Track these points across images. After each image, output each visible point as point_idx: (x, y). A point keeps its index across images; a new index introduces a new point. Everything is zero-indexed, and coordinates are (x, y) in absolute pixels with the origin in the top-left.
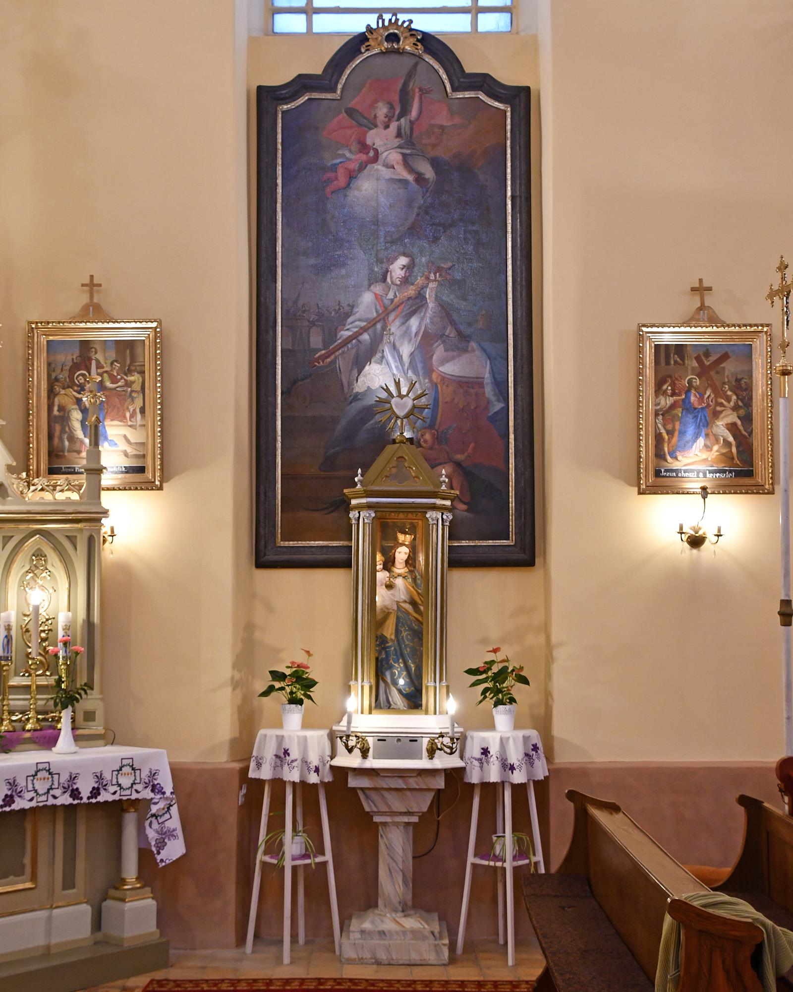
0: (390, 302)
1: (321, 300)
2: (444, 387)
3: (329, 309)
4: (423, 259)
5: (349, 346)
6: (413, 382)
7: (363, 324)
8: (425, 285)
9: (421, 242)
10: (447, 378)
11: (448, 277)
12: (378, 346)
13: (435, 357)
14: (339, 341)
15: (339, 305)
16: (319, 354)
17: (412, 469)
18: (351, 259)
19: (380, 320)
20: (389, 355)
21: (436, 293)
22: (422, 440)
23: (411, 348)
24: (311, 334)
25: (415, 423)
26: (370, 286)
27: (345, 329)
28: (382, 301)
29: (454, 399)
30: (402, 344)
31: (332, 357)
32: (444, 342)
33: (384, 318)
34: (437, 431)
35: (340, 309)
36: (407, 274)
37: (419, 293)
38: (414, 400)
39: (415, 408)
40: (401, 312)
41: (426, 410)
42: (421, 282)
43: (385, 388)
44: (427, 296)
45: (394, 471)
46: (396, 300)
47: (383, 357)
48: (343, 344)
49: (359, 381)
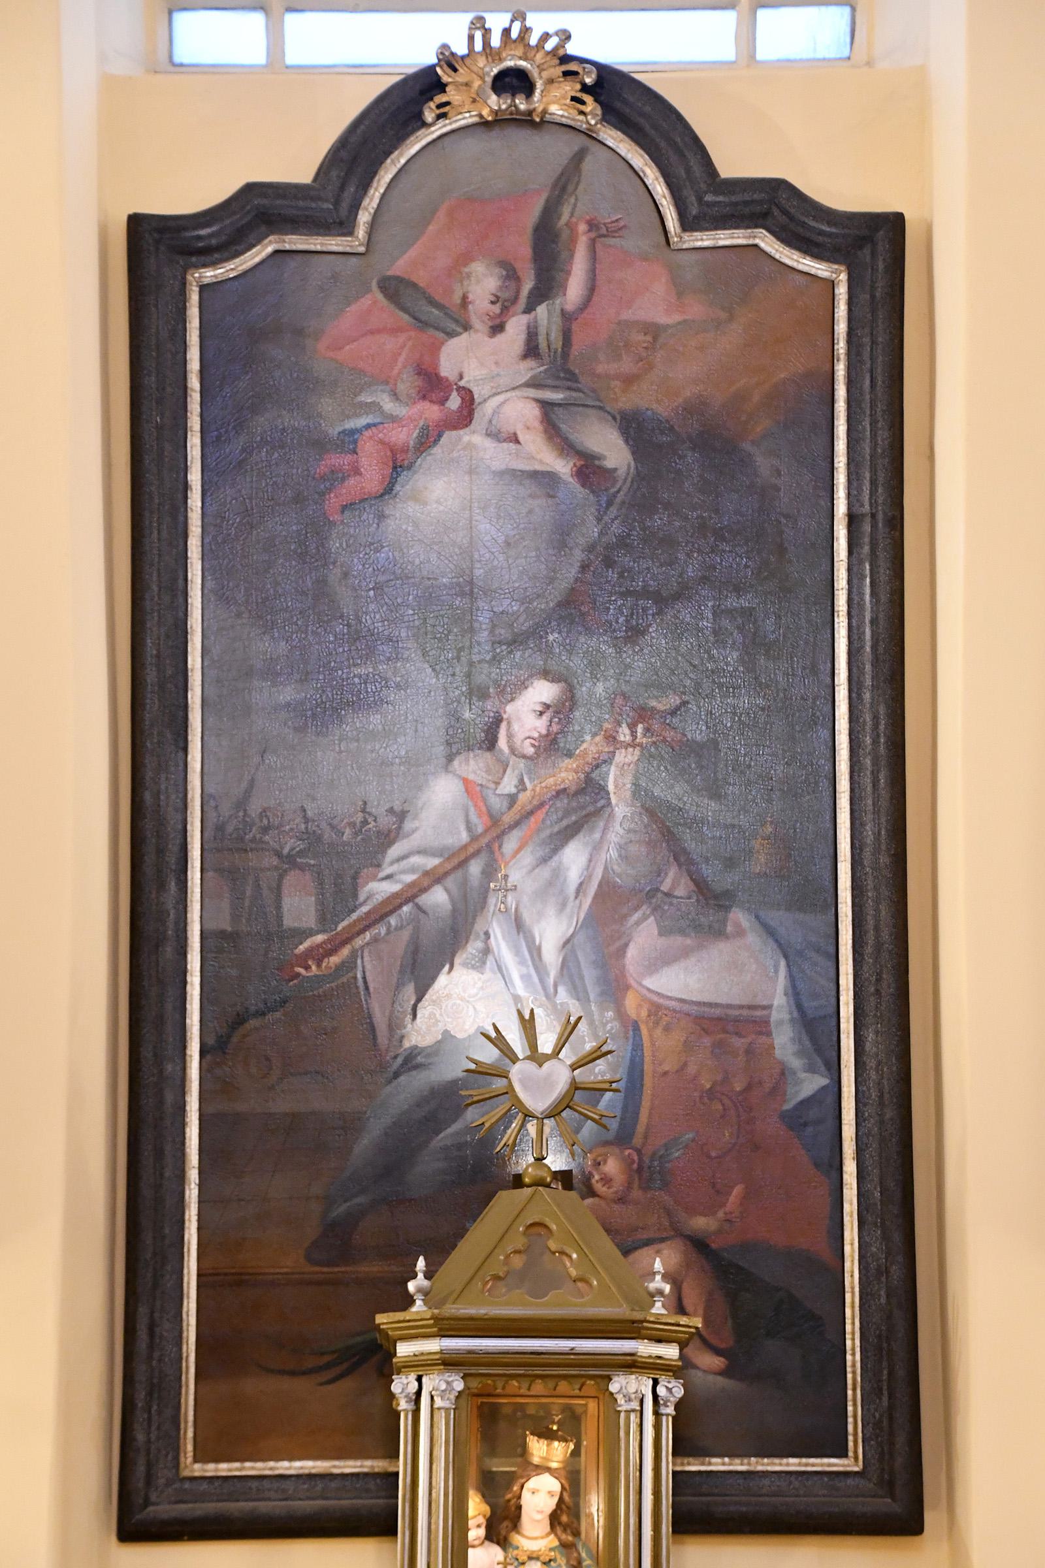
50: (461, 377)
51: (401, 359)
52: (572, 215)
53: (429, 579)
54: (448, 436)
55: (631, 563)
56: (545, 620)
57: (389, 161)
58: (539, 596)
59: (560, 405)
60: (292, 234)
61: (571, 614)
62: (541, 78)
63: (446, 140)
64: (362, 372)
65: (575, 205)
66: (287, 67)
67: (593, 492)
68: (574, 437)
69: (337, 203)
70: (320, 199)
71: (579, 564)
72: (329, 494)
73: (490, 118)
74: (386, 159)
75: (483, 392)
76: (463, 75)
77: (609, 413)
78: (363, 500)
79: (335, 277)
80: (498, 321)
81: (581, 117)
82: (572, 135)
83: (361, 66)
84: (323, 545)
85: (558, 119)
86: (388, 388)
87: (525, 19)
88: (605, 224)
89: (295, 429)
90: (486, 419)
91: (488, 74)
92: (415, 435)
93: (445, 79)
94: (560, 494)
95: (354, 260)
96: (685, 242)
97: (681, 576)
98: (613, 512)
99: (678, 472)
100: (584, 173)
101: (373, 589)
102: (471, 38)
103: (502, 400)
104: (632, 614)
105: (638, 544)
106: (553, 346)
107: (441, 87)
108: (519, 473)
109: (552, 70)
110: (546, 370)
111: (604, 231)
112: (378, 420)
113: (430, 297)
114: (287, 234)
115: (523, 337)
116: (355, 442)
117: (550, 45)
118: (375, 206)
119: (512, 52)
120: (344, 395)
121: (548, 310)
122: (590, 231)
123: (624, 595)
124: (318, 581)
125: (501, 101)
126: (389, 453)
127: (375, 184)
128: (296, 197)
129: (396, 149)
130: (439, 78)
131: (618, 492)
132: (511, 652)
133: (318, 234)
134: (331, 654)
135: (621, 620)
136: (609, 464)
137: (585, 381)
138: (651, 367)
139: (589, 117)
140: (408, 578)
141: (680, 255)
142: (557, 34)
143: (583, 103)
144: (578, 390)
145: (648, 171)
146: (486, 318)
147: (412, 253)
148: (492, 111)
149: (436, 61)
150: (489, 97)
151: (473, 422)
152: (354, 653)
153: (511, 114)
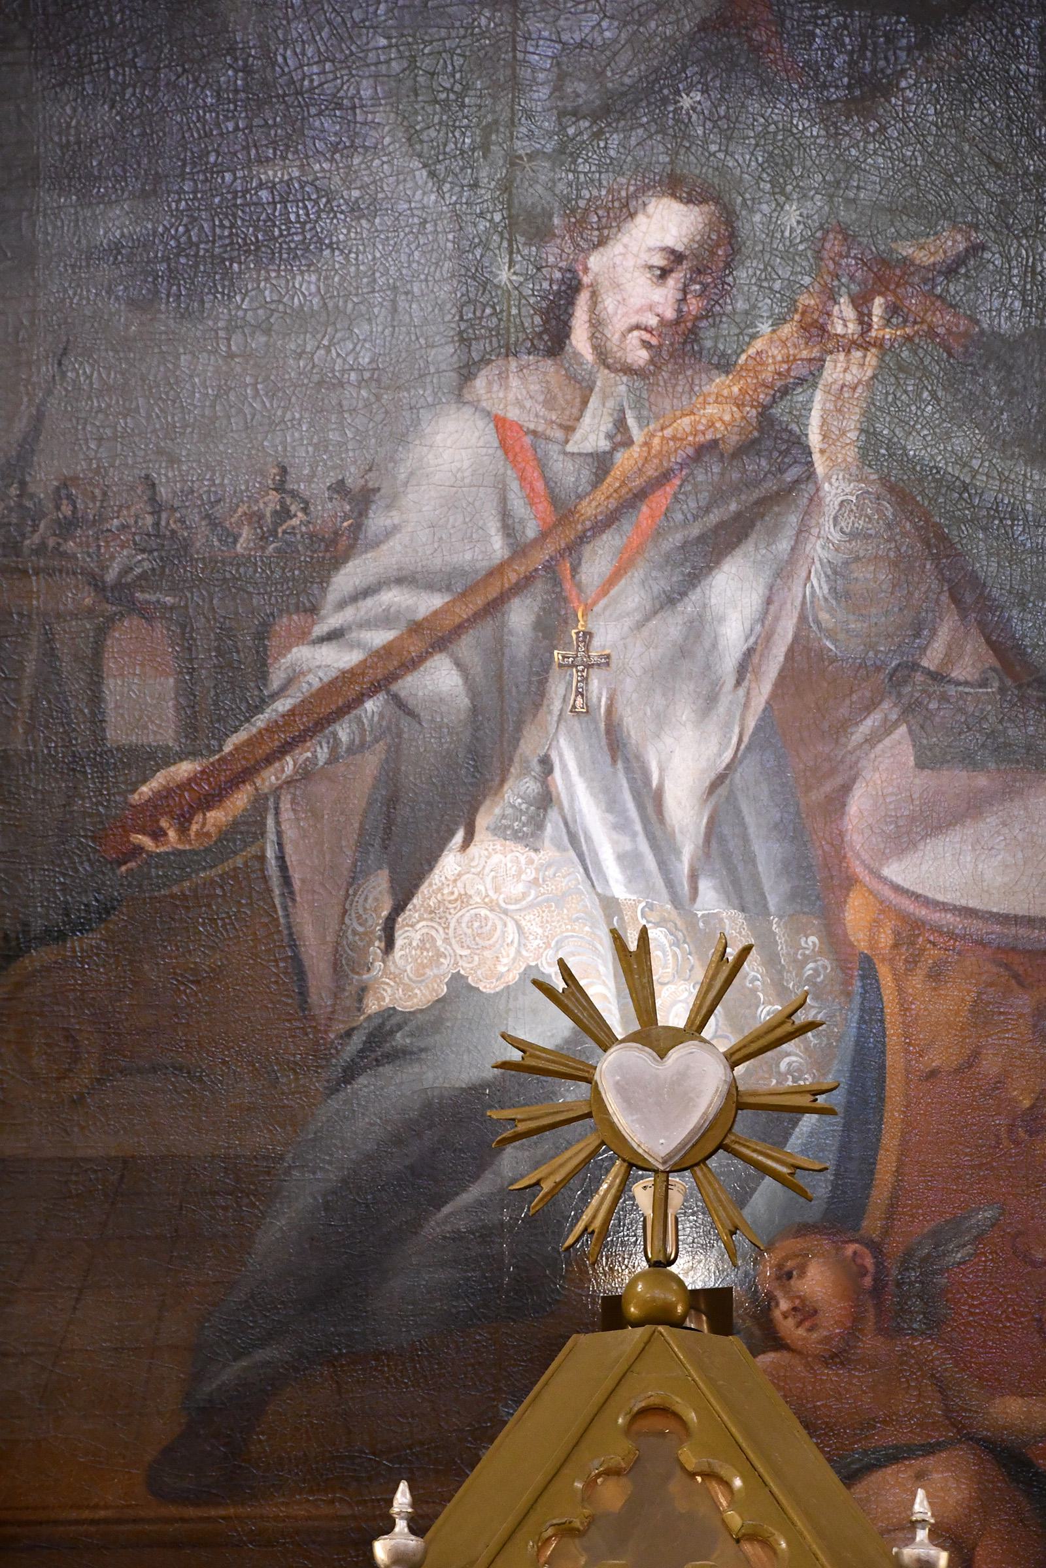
0: (586, 475)
1: (173, 460)
2: (917, 982)
3: (219, 511)
4: (792, 216)
5: (344, 732)
6: (732, 953)
7: (428, 603)
8: (800, 370)
9: (777, 112)
10: (937, 929)
11: (942, 320)
12: (515, 741)
13: (858, 804)
14: (283, 705)
15: (280, 488)
16: (157, 782)
17: (727, 1485)
18: (355, 209)
19: (528, 580)
20: (581, 788)
21: (869, 416)
22: (784, 1305)
23: (713, 748)
24: (110, 665)
25: (741, 1201)
26: (467, 373)
27: (319, 630)
28: (542, 465)
29: (976, 1054)
30: (661, 721)
31: (240, 800)
32: (910, 709)
33: (550, 567)
34: (875, 1248)
35: (283, 514)
36: (694, 306)
37: (765, 418)
38: (734, 1059)
39: (741, 1106)
40: (658, 534)
41: (808, 1121)
42: (777, 352)
43: (560, 985)
44: (814, 439)
45: (613, 1495)
46: (624, 461)
47: (546, 800)
48: (301, 723)
49: (399, 942)
56: (673, 61)
61: (731, 48)
132: (598, 135)
134: (208, 135)
135: (839, 61)
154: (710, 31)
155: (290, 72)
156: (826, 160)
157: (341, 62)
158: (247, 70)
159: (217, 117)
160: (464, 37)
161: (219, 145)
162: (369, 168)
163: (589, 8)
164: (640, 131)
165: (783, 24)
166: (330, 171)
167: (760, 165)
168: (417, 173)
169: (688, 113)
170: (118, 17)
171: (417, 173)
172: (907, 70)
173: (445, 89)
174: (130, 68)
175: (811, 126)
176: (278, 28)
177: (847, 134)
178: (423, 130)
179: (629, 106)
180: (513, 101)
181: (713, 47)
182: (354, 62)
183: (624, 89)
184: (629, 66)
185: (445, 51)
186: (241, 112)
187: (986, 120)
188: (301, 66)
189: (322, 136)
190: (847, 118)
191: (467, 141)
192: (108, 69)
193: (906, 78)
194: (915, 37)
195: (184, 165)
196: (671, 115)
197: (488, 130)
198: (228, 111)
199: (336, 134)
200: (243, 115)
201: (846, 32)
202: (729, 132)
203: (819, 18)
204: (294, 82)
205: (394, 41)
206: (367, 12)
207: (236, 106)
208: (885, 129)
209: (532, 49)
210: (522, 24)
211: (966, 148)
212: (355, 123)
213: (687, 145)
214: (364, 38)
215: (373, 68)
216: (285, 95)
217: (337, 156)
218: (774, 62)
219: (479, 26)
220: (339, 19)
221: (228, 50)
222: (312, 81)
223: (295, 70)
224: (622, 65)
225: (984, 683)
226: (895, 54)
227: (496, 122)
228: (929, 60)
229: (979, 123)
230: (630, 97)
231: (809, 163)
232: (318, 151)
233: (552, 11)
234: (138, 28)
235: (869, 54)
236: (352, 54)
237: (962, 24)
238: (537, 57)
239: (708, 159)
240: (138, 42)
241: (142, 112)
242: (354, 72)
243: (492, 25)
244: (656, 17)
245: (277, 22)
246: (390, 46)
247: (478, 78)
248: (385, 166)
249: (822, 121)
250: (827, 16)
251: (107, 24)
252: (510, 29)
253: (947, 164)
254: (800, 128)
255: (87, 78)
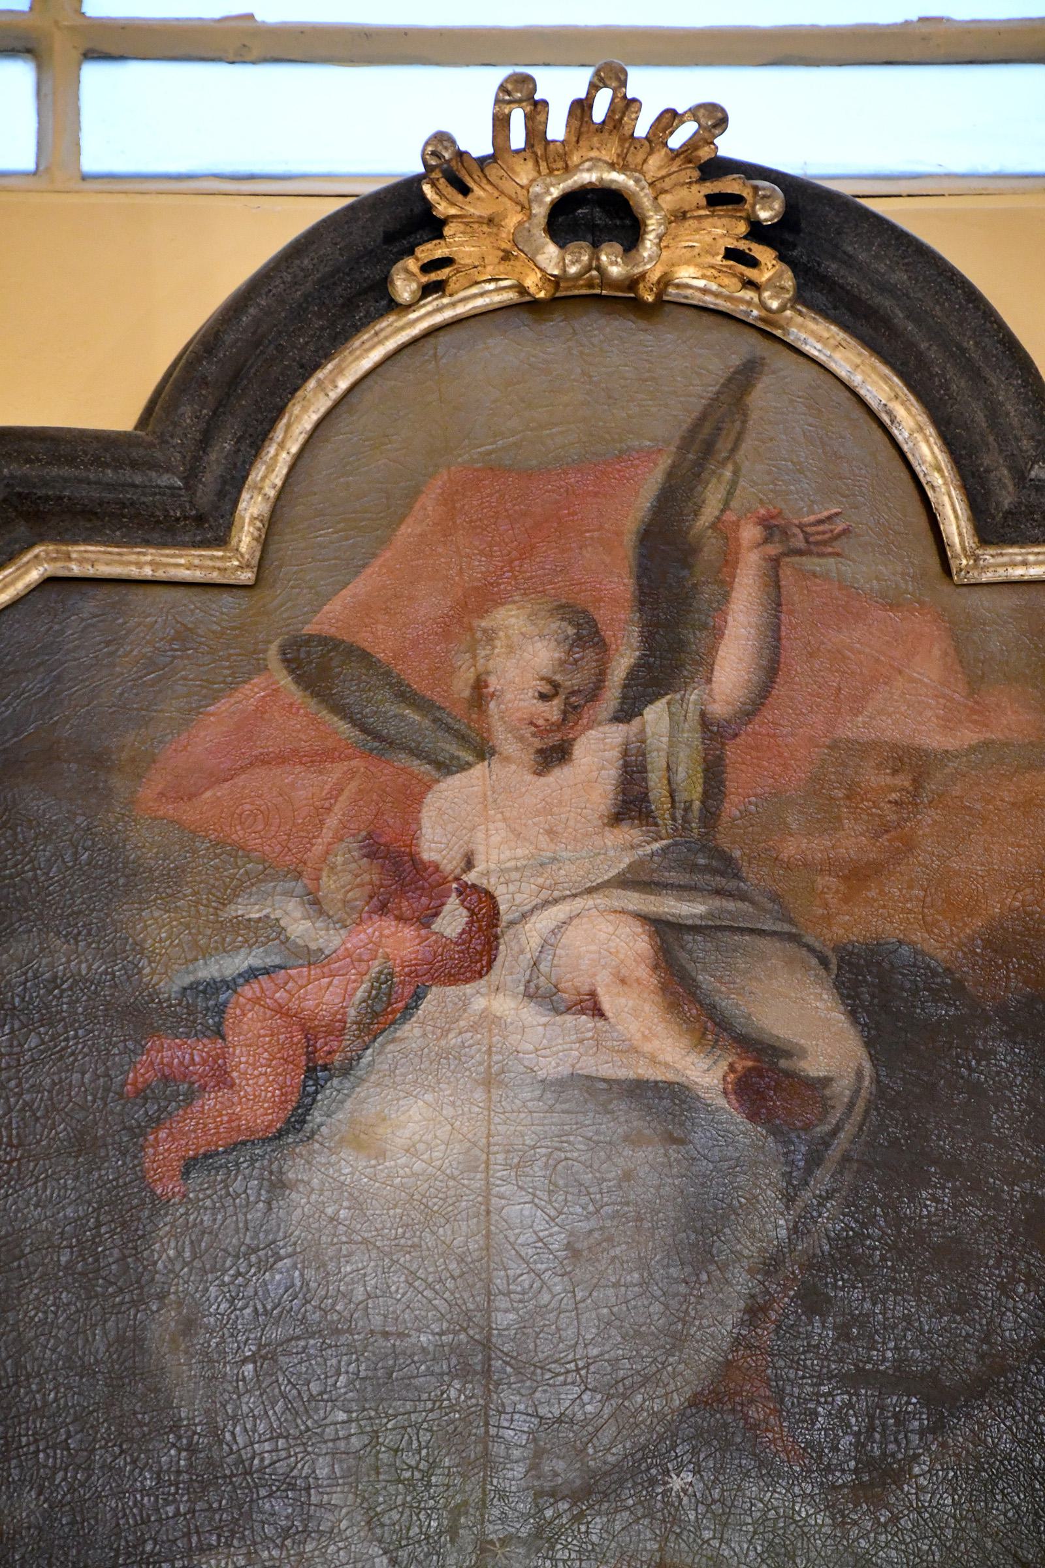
50: (469, 864)
51: (332, 821)
52: (726, 506)
53: (386, 1335)
54: (438, 998)
55: (867, 1305)
56: (661, 1438)
57: (312, 384)
58: (647, 1379)
59: (695, 929)
60: (87, 541)
61: (726, 1425)
62: (658, 208)
63: (444, 338)
64: (240, 850)
65: (734, 484)
66: (85, 178)
67: (775, 1132)
68: (731, 1002)
69: (191, 476)
70: (154, 466)
71: (742, 1305)
72: (156, 1130)
73: (542, 295)
74: (305, 379)
75: (519, 898)
76: (480, 203)
77: (811, 949)
78: (235, 1146)
79: (184, 636)
80: (555, 738)
81: (748, 294)
82: (725, 333)
83: (251, 177)
84: (137, 1254)
85: (697, 299)
86: (299, 888)
87: (624, 84)
88: (801, 526)
89: (78, 980)
90: (526, 959)
91: (538, 198)
92: (360, 994)
93: (442, 209)
94: (698, 1137)
95: (227, 598)
96: (984, 569)
97: (986, 1339)
98: (823, 1179)
99: (976, 1089)
100: (754, 415)
101: (252, 1359)
102: (501, 123)
103: (562, 916)
104: (871, 1429)
105: (883, 1258)
106: (681, 796)
107: (434, 227)
108: (604, 1086)
109: (683, 192)
110: (665, 850)
111: (799, 542)
112: (277, 960)
113: (400, 683)
114: (76, 543)
115: (611, 774)
116: (221, 1010)
117: (678, 139)
118: (279, 482)
119: (593, 154)
120: (198, 902)
121: (671, 714)
122: (766, 540)
123: (858, 1378)
124: (121, 1339)
125: (568, 258)
126: (298, 1037)
127: (279, 434)
128: (97, 461)
129: (328, 357)
130: (428, 206)
131: (834, 1133)
132: (578, 1518)
133: (147, 543)
134: (146, 1521)
135: (845, 1442)
136: (814, 1067)
137: (754, 876)
138: (909, 846)
139: (766, 294)
140: (337, 1332)
141: (982, 601)
142: (694, 112)
143: (753, 263)
144: (743, 897)
145: (900, 412)
146: (527, 731)
147: (360, 586)
148: (546, 278)
149: (421, 169)
150: (539, 250)
151: (492, 972)
152: (200, 1519)
153: (591, 285)
154: (702, 1406)
155: (239, 1450)
156: (833, 1552)
157: (295, 1438)
158: (192, 1449)
159: (157, 1500)
160: (432, 1410)
161: (158, 1532)
162: (324, 1554)
163: (569, 1380)
164: (626, 1514)
165: (782, 1402)
166: (280, 1559)
167: (759, 1555)
168: (377, 1560)
169: (679, 1496)
170: (52, 1395)
171: (377, 1560)
172: (920, 1455)
173: (410, 1467)
174: (62, 1450)
175: (815, 1513)
176: (227, 1402)
177: (855, 1523)
178: (384, 1512)
179: (613, 1486)
180: (484, 1480)
181: (705, 1424)
182: (309, 1438)
183: (608, 1467)
184: (613, 1443)
185: (410, 1426)
186: (183, 1495)
187: (1010, 1514)
188: (252, 1444)
189: (272, 1520)
190: (855, 1506)
191: (434, 1524)
192: (37, 1451)
193: (919, 1464)
194: (928, 1419)
195: (117, 1556)
196: (659, 1497)
197: (458, 1511)
198: (169, 1494)
199: (287, 1517)
200: (185, 1498)
201: (851, 1412)
202: (724, 1518)
203: (822, 1396)
204: (243, 1462)
205: (354, 1415)
206: (325, 1384)
207: (177, 1489)
208: (898, 1519)
209: (506, 1424)
210: (495, 1397)
211: (989, 1545)
212: (310, 1505)
213: (678, 1531)
214: (322, 1412)
215: (330, 1444)
216: (233, 1475)
217: (288, 1542)
218: (773, 1441)
219: (449, 1399)
220: (294, 1392)
221: (171, 1428)
222: (262, 1460)
223: (245, 1448)
224: (606, 1441)
225: (695, 585)
226: (906, 1437)
227: (465, 1503)
228: (943, 1445)
229: (1002, 1517)
230: (615, 1477)
231: (813, 1554)
232: (267, 1538)
233: (528, 1383)
234: (73, 1406)
235: (877, 1436)
236: (308, 1429)
237: (980, 1408)
238: (512, 1433)
239: (701, 1547)
240: (72, 1422)
241: (73, 1498)
242: (310, 1449)
243: (463, 1397)
244: (642, 1390)
245: (226, 1396)
246: (350, 1421)
247: (448, 1454)
248: (341, 1553)
249: (827, 1507)
250: (830, 1394)
251: (39, 1404)
252: (481, 1402)
253: (968, 1561)
254: (804, 1514)
255: (14, 1463)
